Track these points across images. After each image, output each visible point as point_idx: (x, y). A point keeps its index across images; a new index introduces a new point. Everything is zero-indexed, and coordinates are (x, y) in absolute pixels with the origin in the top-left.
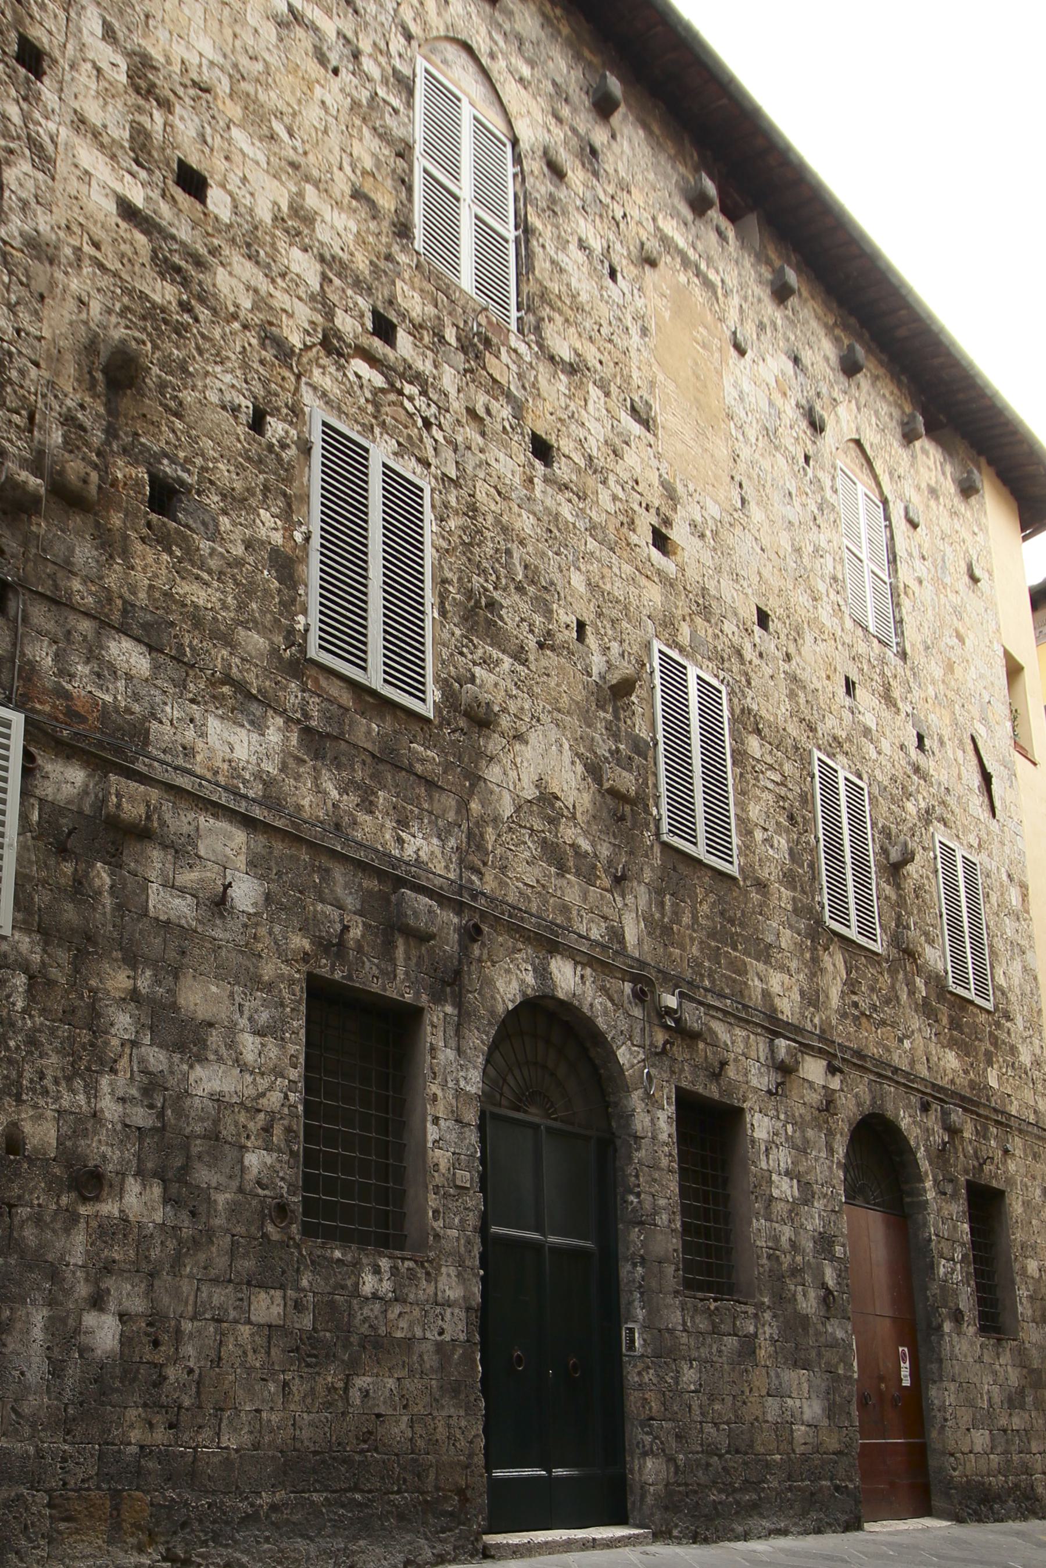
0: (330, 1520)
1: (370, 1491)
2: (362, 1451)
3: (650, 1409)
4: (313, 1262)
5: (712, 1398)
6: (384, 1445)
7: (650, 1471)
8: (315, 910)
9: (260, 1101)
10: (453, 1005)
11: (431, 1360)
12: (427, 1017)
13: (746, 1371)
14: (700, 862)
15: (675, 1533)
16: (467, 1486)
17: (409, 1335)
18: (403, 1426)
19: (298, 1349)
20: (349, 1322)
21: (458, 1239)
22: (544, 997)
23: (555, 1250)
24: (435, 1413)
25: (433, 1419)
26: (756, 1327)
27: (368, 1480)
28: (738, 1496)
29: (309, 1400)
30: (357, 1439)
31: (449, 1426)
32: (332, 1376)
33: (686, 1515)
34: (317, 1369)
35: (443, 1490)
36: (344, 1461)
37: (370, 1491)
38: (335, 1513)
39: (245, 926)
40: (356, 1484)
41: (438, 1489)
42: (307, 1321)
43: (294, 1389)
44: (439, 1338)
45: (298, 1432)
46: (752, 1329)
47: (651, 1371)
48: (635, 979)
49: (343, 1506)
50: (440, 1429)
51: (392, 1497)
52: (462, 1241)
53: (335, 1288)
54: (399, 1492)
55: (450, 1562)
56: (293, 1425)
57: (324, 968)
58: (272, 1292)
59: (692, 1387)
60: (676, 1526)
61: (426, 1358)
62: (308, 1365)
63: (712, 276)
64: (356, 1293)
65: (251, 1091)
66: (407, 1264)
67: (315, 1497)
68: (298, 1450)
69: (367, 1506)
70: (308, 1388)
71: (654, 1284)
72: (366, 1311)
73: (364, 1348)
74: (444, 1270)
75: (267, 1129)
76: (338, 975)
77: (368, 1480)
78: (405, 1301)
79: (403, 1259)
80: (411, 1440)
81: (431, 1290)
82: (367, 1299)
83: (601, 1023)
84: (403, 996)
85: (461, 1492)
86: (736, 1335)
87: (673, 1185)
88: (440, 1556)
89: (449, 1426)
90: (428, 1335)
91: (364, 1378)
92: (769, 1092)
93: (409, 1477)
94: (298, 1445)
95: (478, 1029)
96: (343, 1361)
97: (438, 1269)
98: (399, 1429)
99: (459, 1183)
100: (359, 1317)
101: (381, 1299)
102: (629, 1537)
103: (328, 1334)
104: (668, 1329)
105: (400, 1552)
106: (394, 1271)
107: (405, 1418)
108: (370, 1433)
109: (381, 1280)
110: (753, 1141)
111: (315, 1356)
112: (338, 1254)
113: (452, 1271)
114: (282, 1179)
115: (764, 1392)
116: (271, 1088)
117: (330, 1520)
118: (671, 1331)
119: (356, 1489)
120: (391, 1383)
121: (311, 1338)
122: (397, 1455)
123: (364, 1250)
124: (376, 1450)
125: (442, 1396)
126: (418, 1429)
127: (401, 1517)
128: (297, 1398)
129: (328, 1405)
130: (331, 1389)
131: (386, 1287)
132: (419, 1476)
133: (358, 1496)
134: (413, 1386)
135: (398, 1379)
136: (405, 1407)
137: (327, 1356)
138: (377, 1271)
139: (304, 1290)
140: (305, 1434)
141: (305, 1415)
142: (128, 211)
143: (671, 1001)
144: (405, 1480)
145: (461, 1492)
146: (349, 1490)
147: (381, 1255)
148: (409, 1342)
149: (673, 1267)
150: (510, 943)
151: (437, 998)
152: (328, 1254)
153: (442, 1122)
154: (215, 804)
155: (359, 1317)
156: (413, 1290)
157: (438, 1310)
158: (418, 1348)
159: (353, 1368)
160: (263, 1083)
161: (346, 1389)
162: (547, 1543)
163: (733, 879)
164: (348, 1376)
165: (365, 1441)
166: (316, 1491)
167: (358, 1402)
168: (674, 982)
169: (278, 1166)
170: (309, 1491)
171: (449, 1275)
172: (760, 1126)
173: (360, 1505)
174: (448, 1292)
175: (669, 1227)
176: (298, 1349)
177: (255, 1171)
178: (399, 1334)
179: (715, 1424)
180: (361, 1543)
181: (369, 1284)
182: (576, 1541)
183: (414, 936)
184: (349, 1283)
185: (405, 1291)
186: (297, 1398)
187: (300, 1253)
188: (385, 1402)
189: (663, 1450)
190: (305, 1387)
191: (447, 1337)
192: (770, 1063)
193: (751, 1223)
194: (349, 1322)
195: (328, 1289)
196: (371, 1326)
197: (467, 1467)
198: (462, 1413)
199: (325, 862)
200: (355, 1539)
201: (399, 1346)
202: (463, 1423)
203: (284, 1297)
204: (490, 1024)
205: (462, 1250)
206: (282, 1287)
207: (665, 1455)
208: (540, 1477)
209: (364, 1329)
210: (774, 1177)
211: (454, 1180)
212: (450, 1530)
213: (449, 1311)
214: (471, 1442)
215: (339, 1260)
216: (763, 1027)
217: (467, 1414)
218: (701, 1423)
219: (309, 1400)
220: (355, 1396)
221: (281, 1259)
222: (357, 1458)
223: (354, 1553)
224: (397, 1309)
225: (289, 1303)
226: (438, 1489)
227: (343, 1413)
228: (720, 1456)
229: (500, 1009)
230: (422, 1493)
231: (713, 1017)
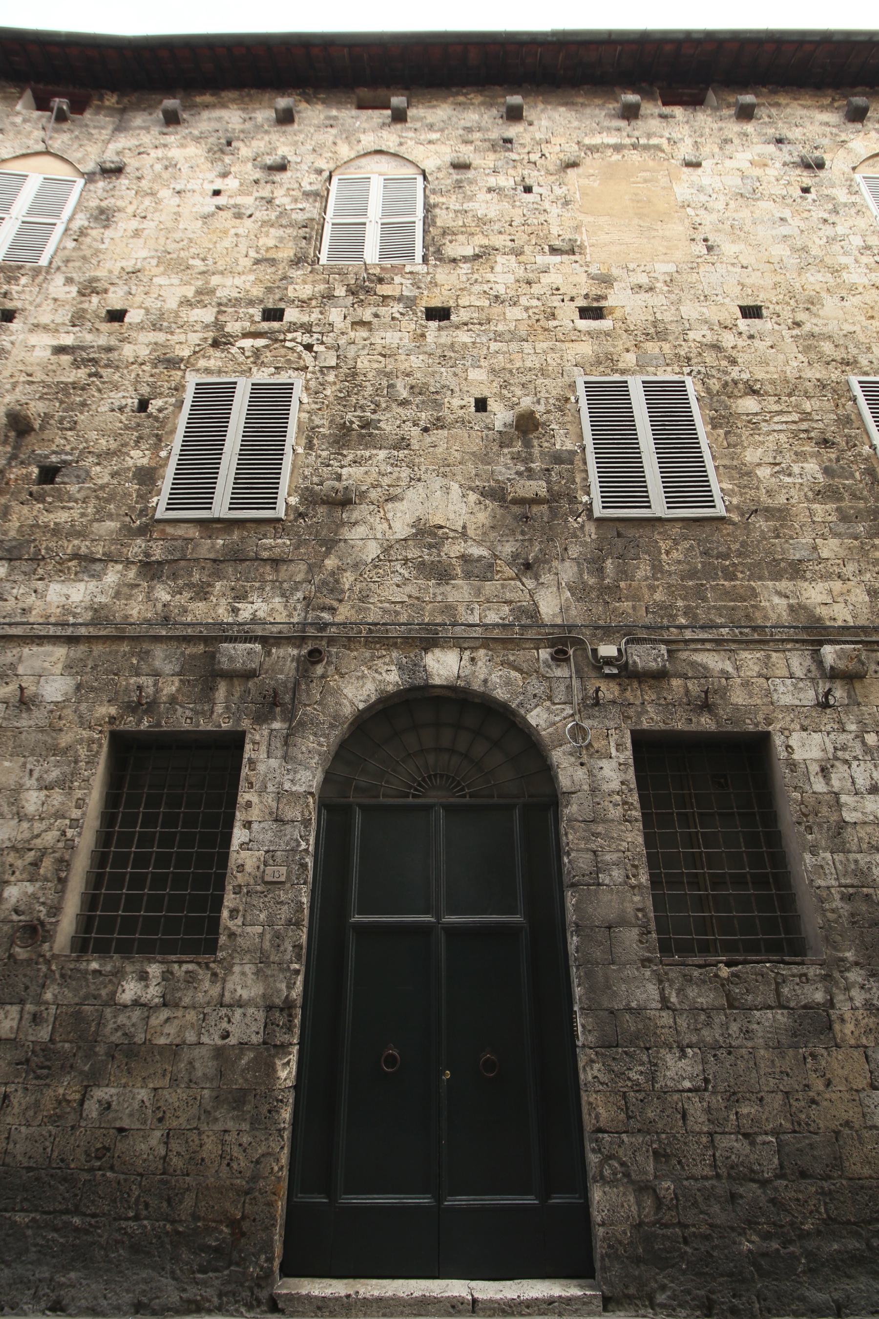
0: (36, 1245)
1: (94, 1216)
2: (91, 1170)
3: (597, 1117)
4: (63, 976)
5: (733, 1098)
6: (124, 1163)
7: (608, 1204)
8: (128, 684)
9: (33, 842)
10: (283, 720)
11: (204, 1066)
12: (248, 737)
13: (814, 1056)
14: (659, 519)
15: (661, 1298)
16: (244, 1218)
17: (178, 1041)
18: (153, 1142)
19: (28, 1061)
20: (97, 1033)
21: (262, 935)
22: (413, 689)
23: (452, 931)
24: (204, 1127)
25: (200, 1134)
26: (828, 991)
27: (93, 1202)
28: (811, 1244)
29: (31, 1113)
30: (88, 1155)
31: (223, 1143)
32: (66, 1087)
33: (684, 1272)
34: (48, 1081)
35: (204, 1219)
36: (65, 1180)
37: (94, 1216)
38: (44, 1238)
39: (51, 711)
40: (77, 1207)
41: (196, 1217)
42: (44, 1033)
43: (15, 1102)
44: (220, 1042)
45: (11, 1146)
46: (819, 996)
47: (596, 1066)
48: (552, 643)
49: (56, 1230)
50: (209, 1146)
51: (123, 1224)
52: (268, 937)
53: (86, 997)
54: (136, 1218)
55: (209, 1312)
56: (8, 1138)
57: (129, 724)
58: (8, 1007)
59: (687, 1084)
60: (663, 1288)
61: (197, 1065)
62: (38, 1077)
63: (654, 141)
64: (111, 1001)
65: (27, 835)
66: (185, 967)
67: (18, 1218)
68: (8, 1165)
69: (87, 1232)
70: (32, 1100)
71: (598, 954)
72: (122, 1019)
73: (113, 1057)
74: (237, 969)
75: (36, 864)
76: (145, 725)
77: (93, 1202)
78: (177, 1006)
79: (180, 963)
80: (164, 1158)
81: (215, 991)
82: (126, 1006)
83: (501, 694)
84: (220, 726)
85: (234, 1224)
86: (782, 1007)
87: (634, 837)
88: (189, 1301)
89: (223, 1143)
90: (205, 1039)
91: (106, 1090)
92: (819, 704)
93: (153, 1202)
94: (8, 1160)
95: (315, 735)
96: (81, 1072)
97: (229, 970)
98: (148, 1145)
99: (267, 879)
100: (111, 1026)
101: (144, 1005)
102: (569, 1301)
103: (67, 1045)
104: (629, 1009)
105: (128, 1291)
106: (167, 976)
107: (158, 1134)
108: (108, 1149)
109: (147, 986)
110: (793, 766)
111: (49, 1068)
112: (94, 965)
113: (249, 969)
114: (43, 904)
115: (861, 1083)
116: (49, 829)
117: (36, 1245)
118: (638, 1012)
119: (77, 1211)
120: (143, 1094)
121: (46, 1050)
122: (141, 1175)
123: (128, 958)
124: (112, 1168)
125: (216, 1108)
126: (174, 1145)
127: (135, 1249)
128: (16, 1111)
129: (55, 1119)
130: (61, 1101)
131: (153, 993)
132: (169, 1201)
133: (76, 1220)
134: (173, 1097)
135: (155, 1089)
136: (160, 1120)
137: (62, 1067)
138: (143, 977)
139: (47, 1003)
140: (19, 1149)
141: (23, 1129)
142: (60, 350)
143: (608, 650)
144: (147, 1206)
145: (234, 1224)
146: (67, 1212)
147: (150, 961)
148: (175, 1050)
149: (635, 931)
150: (368, 654)
151: (261, 718)
152: (83, 966)
153: (255, 826)
154: (39, 637)
155: (111, 1026)
156: (190, 993)
157: (224, 1011)
158: (186, 1055)
159: (93, 1079)
160: (38, 827)
161: (82, 1103)
162: (380, 1300)
163: (722, 519)
164: (87, 1087)
165: (98, 1158)
166: (22, 1210)
167: (94, 1115)
168: (608, 633)
169: (40, 894)
170: (13, 1210)
171: (243, 974)
172: (804, 747)
173: (77, 1229)
174: (240, 991)
175: (626, 883)
176: (28, 1061)
177: (13, 900)
178: (162, 1041)
179: (746, 1135)
180: (73, 1275)
181: (130, 990)
182: (436, 1301)
183: (237, 676)
184: (104, 992)
185: (178, 995)
186: (16, 1111)
187: (49, 969)
188: (131, 1115)
189: (627, 1175)
190: (30, 1099)
191: (232, 1041)
192: (815, 673)
193: (802, 859)
194: (97, 1033)
195: (77, 1000)
196: (125, 1034)
197: (247, 1193)
198: (245, 1126)
199: (145, 646)
200: (66, 1269)
201: (160, 1054)
202: (245, 1139)
203: (21, 1012)
204: (332, 726)
205: (267, 945)
206: (22, 1002)
207: (632, 1182)
208: (418, 1207)
209: (117, 1038)
210: (844, 798)
211: (263, 878)
212: (216, 1270)
213: (239, 1012)
214: (258, 1162)
215: (95, 972)
216: (797, 641)
217: (253, 1129)
218: (711, 1134)
219: (31, 1113)
220: (92, 1109)
221: (25, 976)
222: (85, 1176)
223: (61, 1286)
224: (165, 1014)
225: (26, 1016)
226: (196, 1217)
227: (73, 1127)
228: (764, 1183)
229: (347, 710)
230: (173, 1222)
231: (696, 650)
